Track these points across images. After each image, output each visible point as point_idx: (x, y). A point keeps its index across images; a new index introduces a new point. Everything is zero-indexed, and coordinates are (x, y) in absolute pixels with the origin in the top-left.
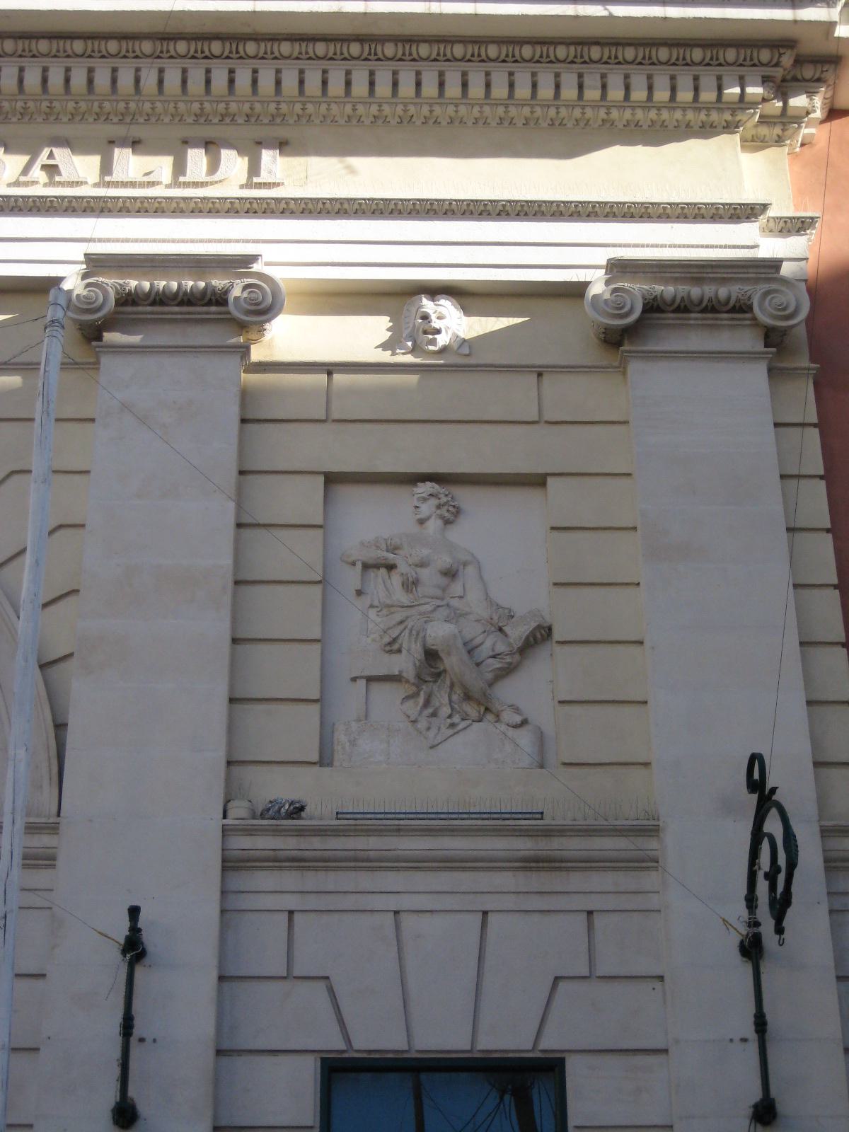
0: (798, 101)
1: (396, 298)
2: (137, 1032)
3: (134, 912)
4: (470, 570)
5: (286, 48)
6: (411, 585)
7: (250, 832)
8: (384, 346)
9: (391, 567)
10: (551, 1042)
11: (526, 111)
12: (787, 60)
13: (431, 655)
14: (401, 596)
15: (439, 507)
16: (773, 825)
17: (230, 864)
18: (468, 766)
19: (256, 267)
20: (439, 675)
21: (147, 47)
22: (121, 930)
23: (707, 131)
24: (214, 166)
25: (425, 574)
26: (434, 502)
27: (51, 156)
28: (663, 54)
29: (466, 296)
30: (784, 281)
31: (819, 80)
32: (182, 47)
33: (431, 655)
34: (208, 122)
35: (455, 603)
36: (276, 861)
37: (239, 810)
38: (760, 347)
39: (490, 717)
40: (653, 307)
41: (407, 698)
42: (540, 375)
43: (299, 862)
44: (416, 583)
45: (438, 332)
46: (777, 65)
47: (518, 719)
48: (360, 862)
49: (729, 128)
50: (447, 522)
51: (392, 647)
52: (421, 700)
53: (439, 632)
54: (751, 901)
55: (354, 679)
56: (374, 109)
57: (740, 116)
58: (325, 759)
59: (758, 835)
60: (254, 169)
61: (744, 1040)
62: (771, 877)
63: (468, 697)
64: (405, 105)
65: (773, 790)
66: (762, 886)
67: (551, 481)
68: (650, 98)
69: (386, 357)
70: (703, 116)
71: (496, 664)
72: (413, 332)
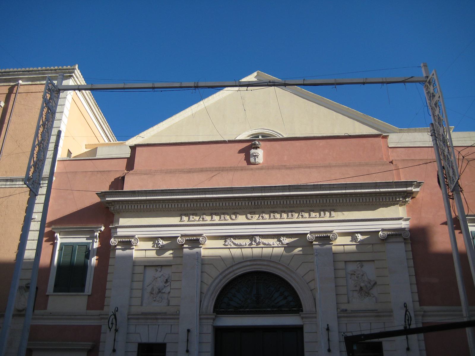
0: (407, 199)
1: (352, 234)
2: (116, 340)
3: (328, 325)
4: (365, 274)
5: (334, 196)
6: (357, 277)
7: (340, 313)
8: (351, 241)
9: (354, 274)
10: (165, 341)
11: (368, 203)
12: (405, 194)
13: (361, 287)
14: (356, 278)
15: (360, 265)
16: (408, 313)
17: (338, 317)
18: (366, 303)
19: (333, 232)
20: (362, 290)
21: (314, 197)
22: (326, 327)
23: (394, 205)
24: (325, 214)
25: (359, 275)
26: (359, 265)
27: (302, 213)
28: (388, 194)
29: (362, 233)
30: (406, 231)
31: (410, 196)
32: (319, 197)
33: (361, 287)
34: (323, 207)
35: (363, 279)
36: (344, 317)
37: (339, 310)
38: (403, 240)
39: (369, 295)
40: (388, 235)
41: (358, 293)
42: (372, 245)
43: (347, 317)
44: (358, 277)
45: (358, 239)
46: (404, 195)
47: (373, 296)
48: (354, 317)
49: (397, 204)
50: (361, 267)
51: (356, 286)
52: (360, 293)
53: (362, 285)
54: (405, 322)
55: (351, 291)
56: (346, 204)
57: (399, 202)
58: (348, 302)
59: (406, 314)
60: (330, 214)
61: (405, 340)
62: (408, 320)
63: (366, 293)
64: (351, 203)
65: (408, 310)
66: (407, 321)
67: (375, 261)
68: (386, 201)
69: (351, 243)
70: (394, 203)
71: (369, 288)
72: (354, 239)
